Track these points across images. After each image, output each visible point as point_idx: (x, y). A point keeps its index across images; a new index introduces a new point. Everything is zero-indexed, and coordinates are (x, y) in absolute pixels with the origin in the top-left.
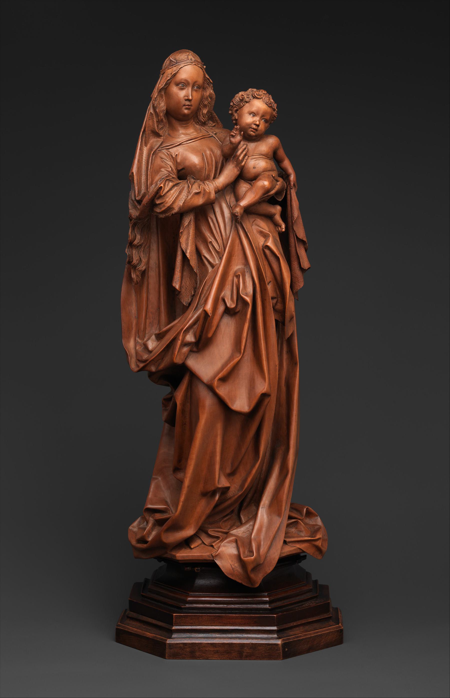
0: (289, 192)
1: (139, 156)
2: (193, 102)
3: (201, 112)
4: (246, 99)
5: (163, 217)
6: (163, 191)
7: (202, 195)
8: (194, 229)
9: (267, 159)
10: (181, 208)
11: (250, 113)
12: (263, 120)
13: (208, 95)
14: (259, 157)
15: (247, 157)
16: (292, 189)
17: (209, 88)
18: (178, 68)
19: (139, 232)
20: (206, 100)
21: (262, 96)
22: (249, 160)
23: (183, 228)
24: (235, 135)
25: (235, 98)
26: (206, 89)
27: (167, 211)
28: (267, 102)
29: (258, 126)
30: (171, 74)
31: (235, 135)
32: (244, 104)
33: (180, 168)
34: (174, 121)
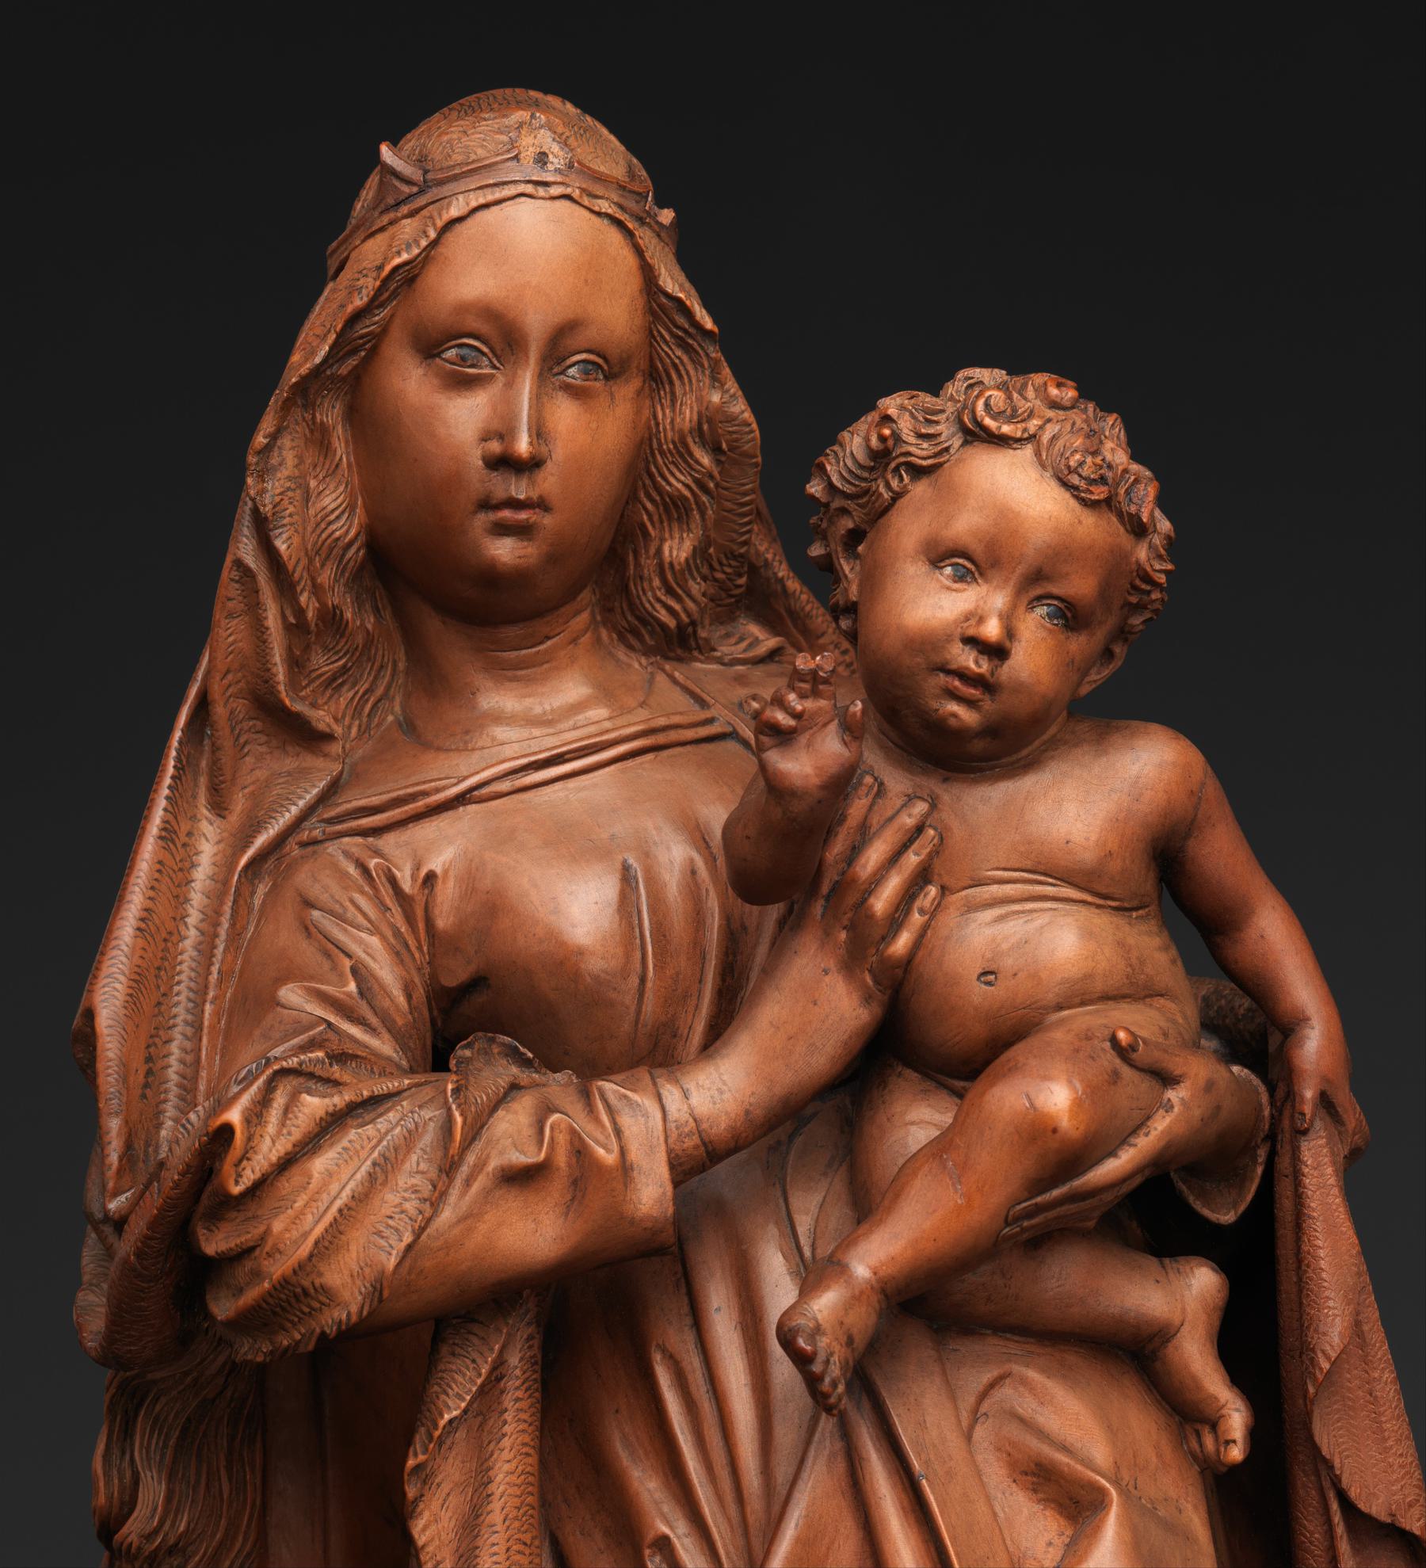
0: (1284, 1163)
1: (152, 888)
2: (548, 482)
3: (647, 551)
4: (912, 449)
5: (260, 1359)
6: (244, 1157)
7: (557, 1188)
8: (525, 1444)
9: (1098, 906)
10: (386, 1294)
11: (939, 555)
12: (1042, 610)
13: (687, 425)
14: (1026, 895)
15: (933, 891)
16: (1305, 1132)
17: (692, 372)
18: (434, 225)
19: (162, 1456)
20: (673, 463)
21: (1034, 424)
22: (949, 919)
23: (430, 1437)
24: (792, 722)
25: (841, 445)
26: (671, 383)
27: (275, 1313)
28: (1069, 467)
29: (997, 652)
30: (380, 268)
31: (792, 722)
32: (895, 484)
33: (456, 974)
34: (433, 625)
